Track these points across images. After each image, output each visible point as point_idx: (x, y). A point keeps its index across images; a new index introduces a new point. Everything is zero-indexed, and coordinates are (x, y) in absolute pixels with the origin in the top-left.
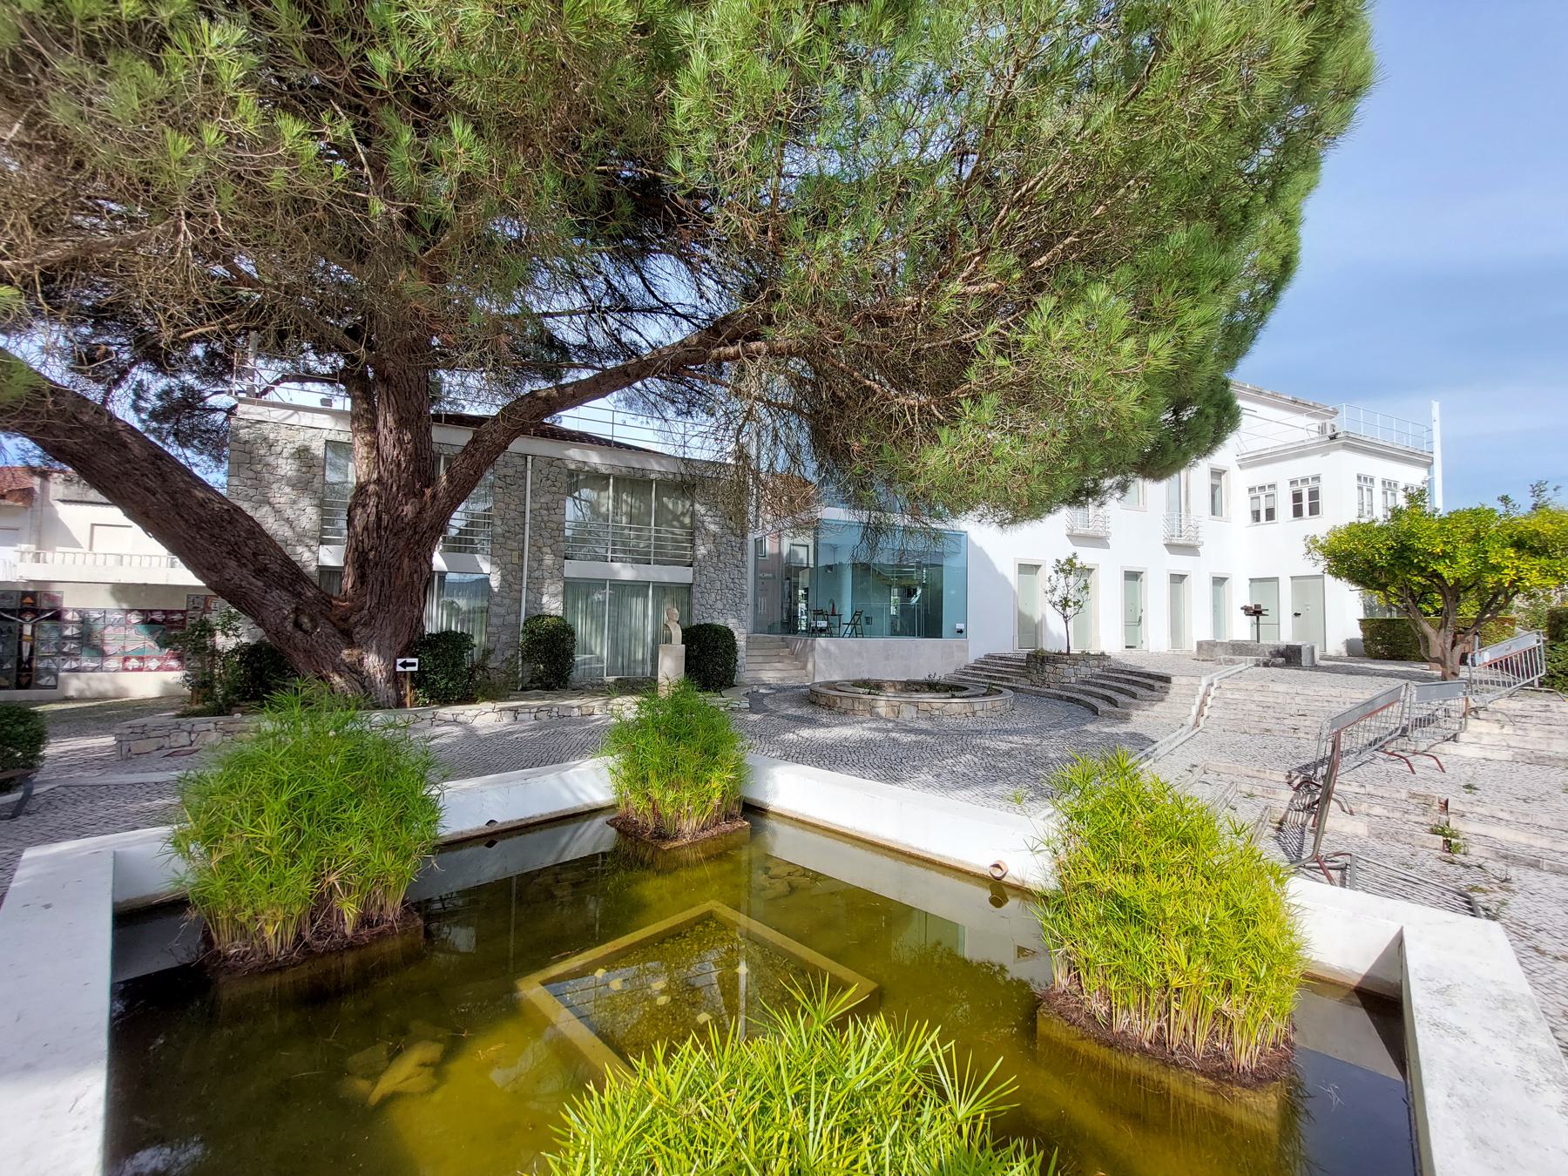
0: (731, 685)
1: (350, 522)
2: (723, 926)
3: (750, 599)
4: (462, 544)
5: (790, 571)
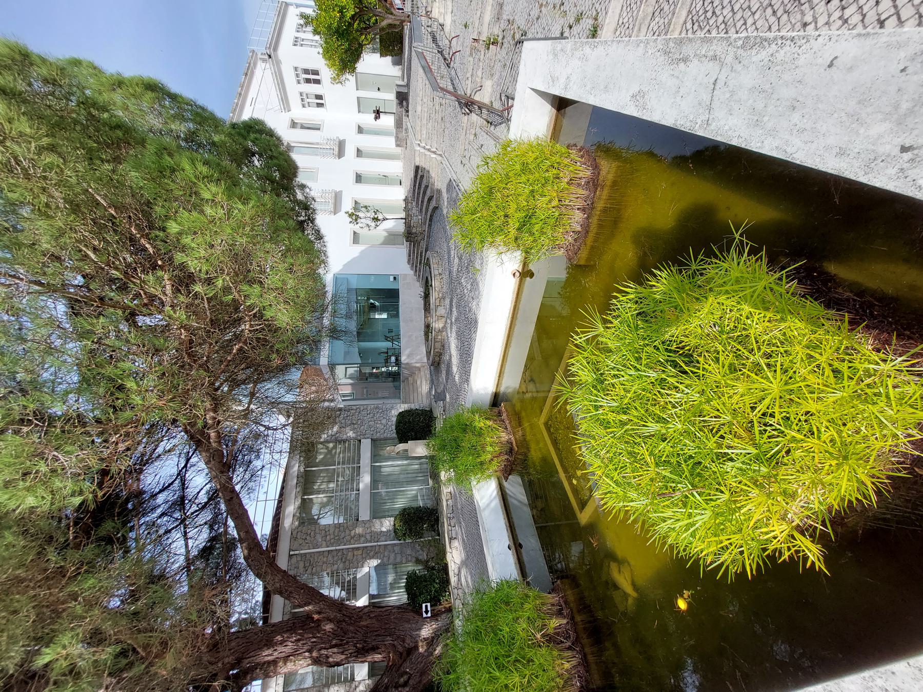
0: (431, 411)
1: (338, 664)
2: (550, 418)
3: (380, 402)
4: (352, 589)
5: (362, 378)
